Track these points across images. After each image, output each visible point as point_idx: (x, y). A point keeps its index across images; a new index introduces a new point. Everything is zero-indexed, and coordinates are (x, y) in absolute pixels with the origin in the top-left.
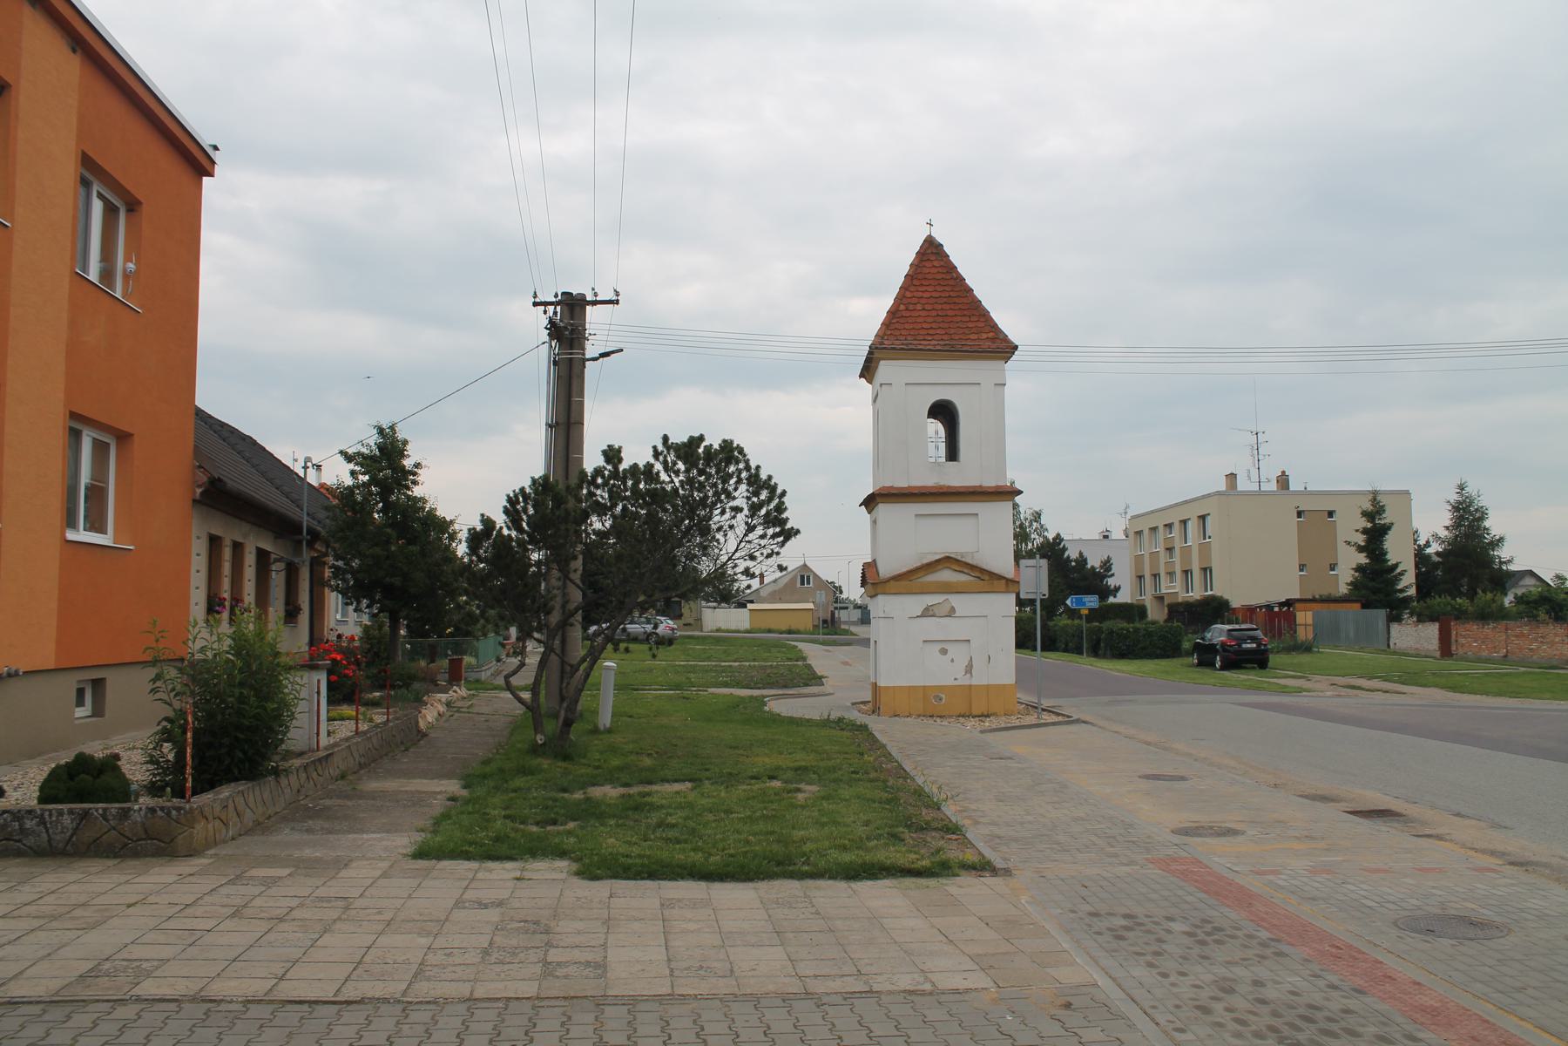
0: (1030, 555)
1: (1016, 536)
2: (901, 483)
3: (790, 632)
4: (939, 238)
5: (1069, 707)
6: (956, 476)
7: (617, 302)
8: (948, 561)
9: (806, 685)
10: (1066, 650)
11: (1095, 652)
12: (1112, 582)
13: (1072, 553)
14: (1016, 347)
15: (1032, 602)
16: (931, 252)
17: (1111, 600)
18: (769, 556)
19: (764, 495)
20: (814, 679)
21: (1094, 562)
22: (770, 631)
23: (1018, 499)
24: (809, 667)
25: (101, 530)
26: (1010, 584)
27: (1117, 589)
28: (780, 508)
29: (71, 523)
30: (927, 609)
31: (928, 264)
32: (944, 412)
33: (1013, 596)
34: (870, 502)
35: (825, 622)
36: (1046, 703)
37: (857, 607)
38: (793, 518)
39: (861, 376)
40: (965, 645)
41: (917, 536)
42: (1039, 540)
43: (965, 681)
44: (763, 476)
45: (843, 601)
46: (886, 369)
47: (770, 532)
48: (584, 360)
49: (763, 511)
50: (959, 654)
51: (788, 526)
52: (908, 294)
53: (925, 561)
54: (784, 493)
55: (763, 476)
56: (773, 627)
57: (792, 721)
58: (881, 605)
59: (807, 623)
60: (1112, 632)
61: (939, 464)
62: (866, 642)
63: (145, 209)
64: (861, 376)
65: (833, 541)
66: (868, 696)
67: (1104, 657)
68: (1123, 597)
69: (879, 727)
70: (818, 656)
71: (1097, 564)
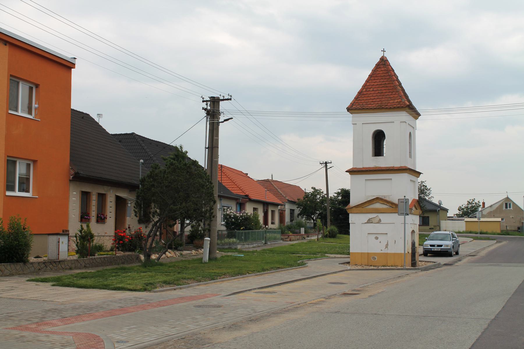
3: (481, 233)
7: (231, 99)
8: (378, 199)
22: (494, 234)
25: (27, 191)
29: (11, 188)
30: (369, 220)
31: (379, 70)
40: (385, 235)
48: (218, 123)
56: (472, 230)
63: (41, 86)
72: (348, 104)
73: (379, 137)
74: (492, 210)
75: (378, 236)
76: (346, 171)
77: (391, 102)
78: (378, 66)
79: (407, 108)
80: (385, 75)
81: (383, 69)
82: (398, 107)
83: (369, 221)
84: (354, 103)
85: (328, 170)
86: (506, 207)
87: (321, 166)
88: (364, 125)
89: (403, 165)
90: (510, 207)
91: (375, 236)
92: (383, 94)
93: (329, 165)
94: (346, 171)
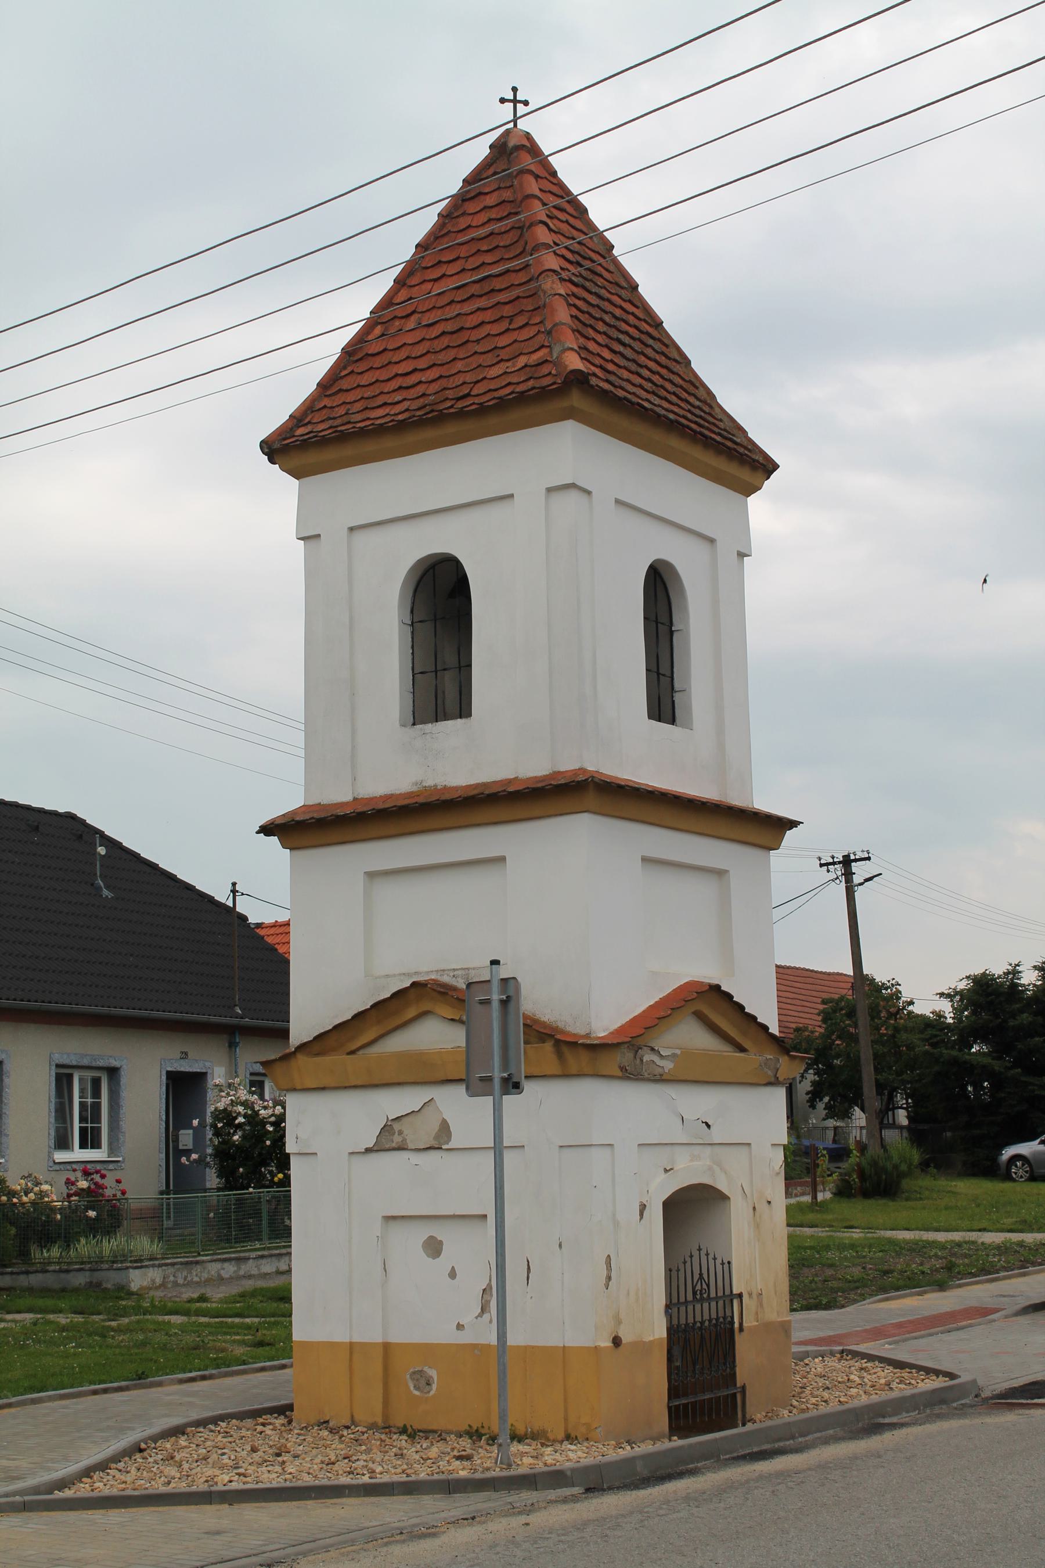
8: (419, 997)
30: (387, 1129)
72: (275, 417)
73: (441, 596)
76: (267, 830)
79: (576, 399)
82: (522, 399)
83: (389, 1139)
85: (859, 894)
87: (823, 875)
88: (360, 537)
89: (568, 762)
91: (422, 1233)
93: (860, 871)
94: (267, 830)
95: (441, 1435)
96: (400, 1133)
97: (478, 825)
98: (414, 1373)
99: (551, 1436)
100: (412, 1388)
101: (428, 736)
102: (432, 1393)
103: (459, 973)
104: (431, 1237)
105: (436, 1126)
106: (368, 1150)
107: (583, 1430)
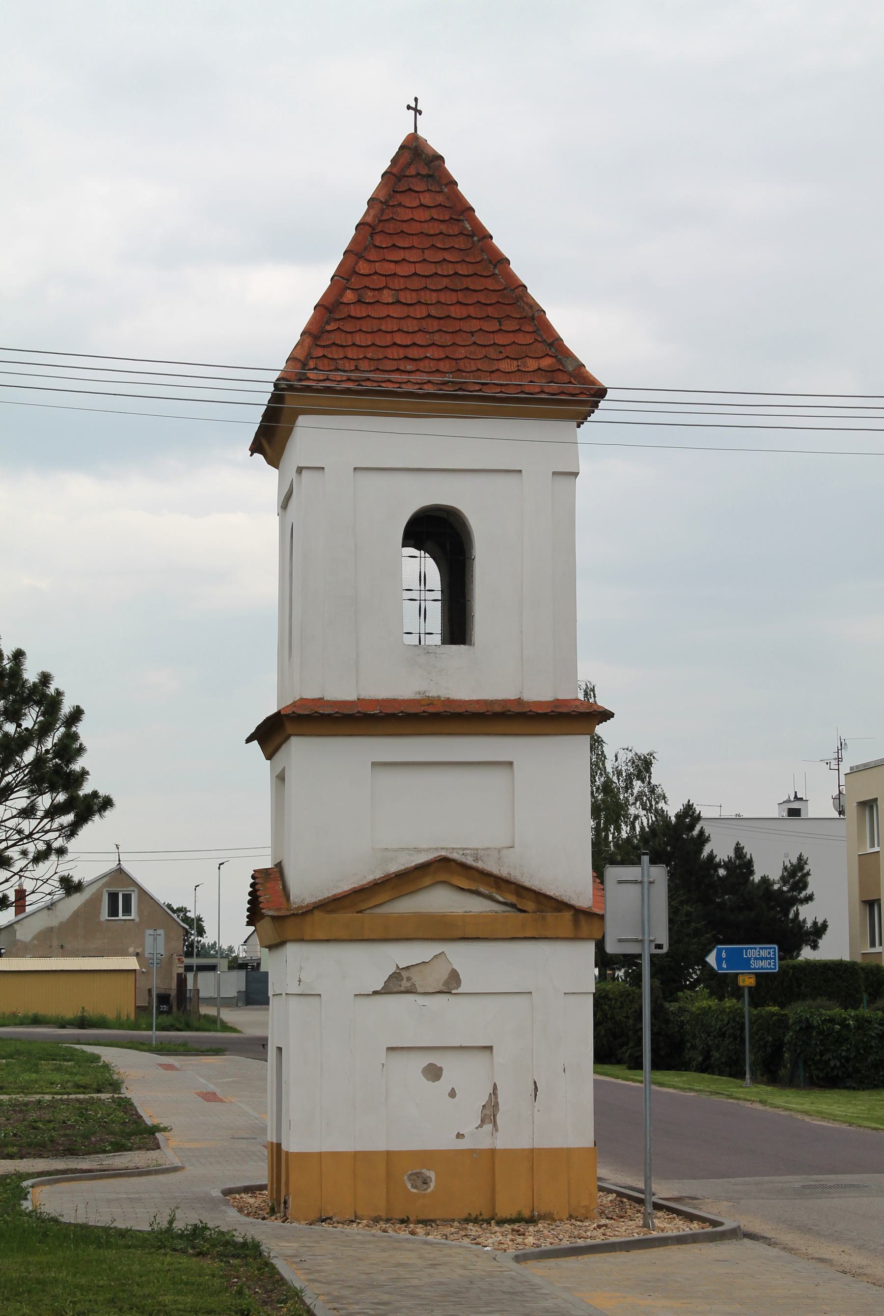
0: (628, 854)
1: (596, 810)
2: (340, 689)
3: (83, 1023)
4: (436, 143)
5: (717, 1201)
6: (464, 678)
8: (444, 869)
9: (119, 1148)
10: (705, 1068)
11: (771, 1072)
12: (807, 914)
13: (720, 848)
14: (601, 393)
15: (630, 960)
16: (417, 179)
17: (807, 954)
18: (40, 857)
19: (31, 719)
20: (139, 1134)
21: (768, 867)
22: (36, 1021)
23: (601, 729)
24: (126, 1105)
26: (582, 921)
27: (820, 930)
28: (69, 748)
30: (396, 977)
31: (409, 201)
32: (439, 534)
33: (589, 950)
34: (271, 734)
35: (163, 999)
36: (663, 1190)
37: (236, 965)
38: (98, 771)
39: (256, 448)
41: (373, 812)
42: (645, 820)
43: (483, 1140)
44: (31, 675)
45: (204, 951)
46: (311, 435)
47: (45, 802)
49: (29, 756)
50: (467, 1078)
51: (86, 789)
52: (363, 268)
53: (394, 868)
54: (77, 715)
55: (31, 675)
56: (93, 1010)
57: (86, 1236)
58: (293, 967)
59: (121, 1002)
60: (807, 1027)
61: (428, 651)
62: (258, 1047)
64: (256, 448)
65: (186, 816)
66: (259, 1172)
67: (790, 1083)
68: (834, 948)
69: (285, 1246)
70: (147, 1080)
71: (775, 874)
74: (55, 923)
75: (437, 1059)
77: (505, 366)
78: (395, 178)
80: (443, 228)
81: (426, 199)
84: (309, 356)
86: (113, 912)
90: (127, 910)
91: (425, 1060)
92: (451, 326)
95: (448, 1222)
96: (409, 979)
97: (488, 734)
98: (411, 1175)
99: (556, 1217)
100: (409, 1187)
101: (432, 655)
102: (429, 1190)
103: (469, 852)
104: (431, 1065)
105: (445, 975)
106: (375, 993)
107: (583, 1211)
